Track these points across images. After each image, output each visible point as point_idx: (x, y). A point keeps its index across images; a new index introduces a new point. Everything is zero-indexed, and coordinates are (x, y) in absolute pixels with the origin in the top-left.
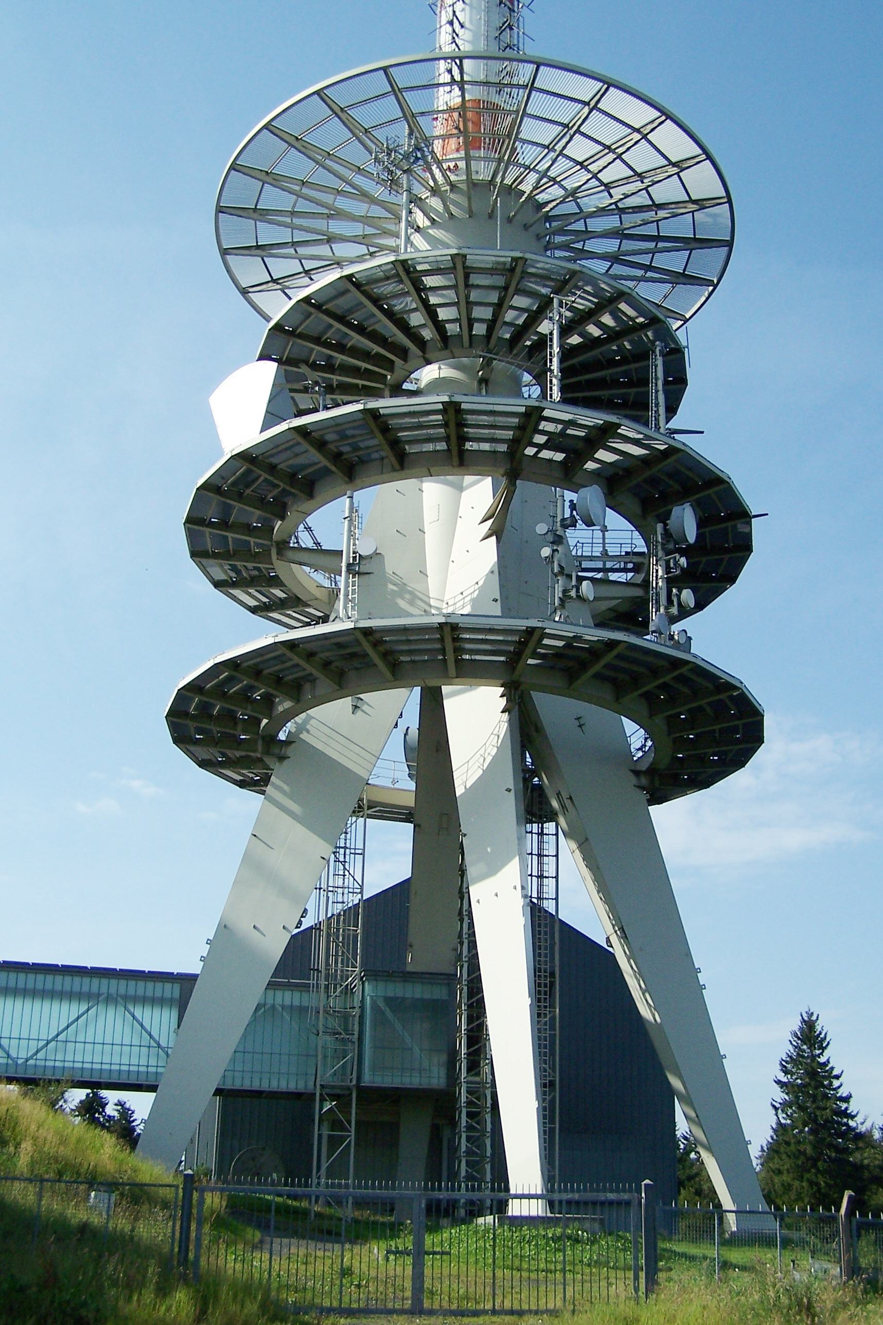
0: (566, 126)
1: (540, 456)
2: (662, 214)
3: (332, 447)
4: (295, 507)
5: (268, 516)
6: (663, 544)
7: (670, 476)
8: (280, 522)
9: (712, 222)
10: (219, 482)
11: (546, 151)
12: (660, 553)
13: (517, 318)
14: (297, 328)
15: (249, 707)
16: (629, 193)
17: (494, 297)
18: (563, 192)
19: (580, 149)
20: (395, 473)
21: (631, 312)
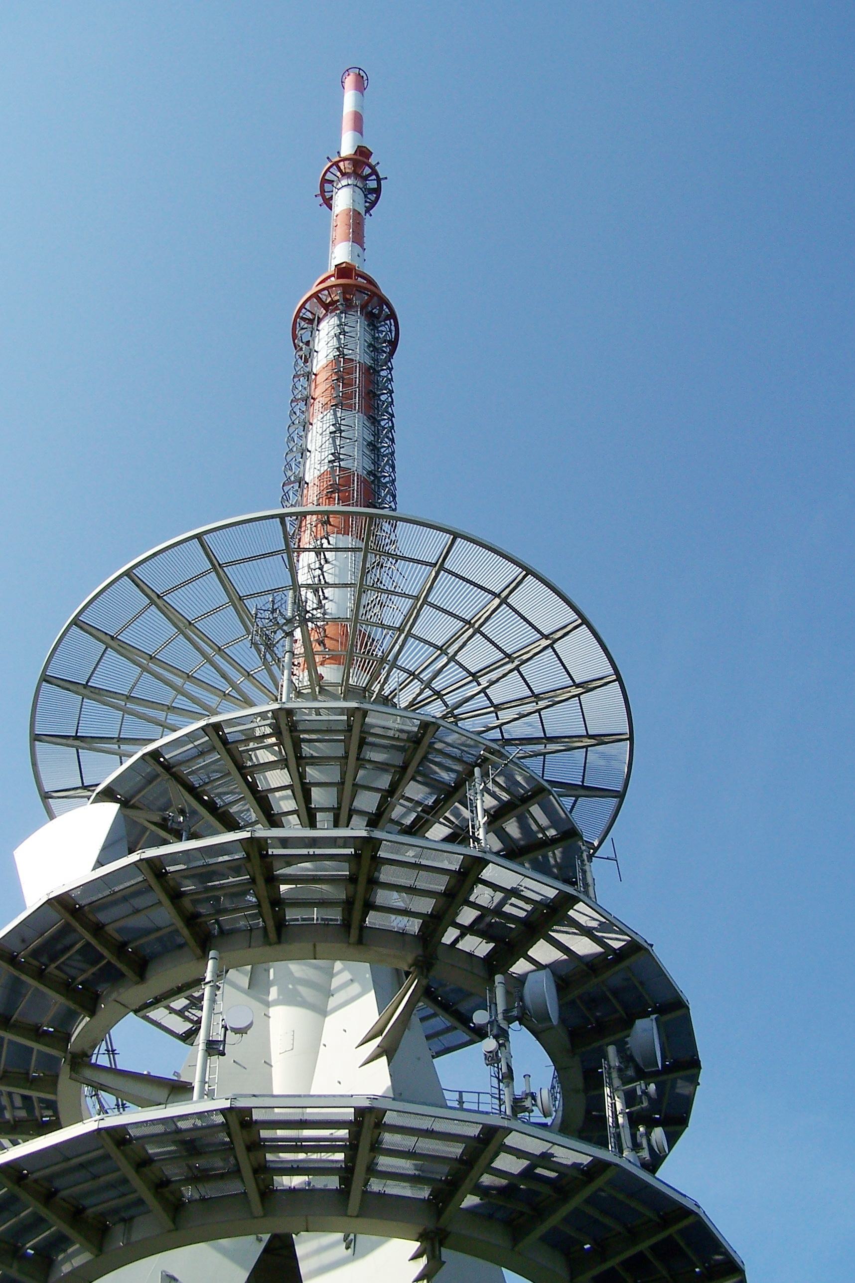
0: (468, 622)
1: (460, 946)
2: (552, 747)
3: (186, 902)
4: (114, 995)
5: (73, 1006)
6: (620, 1070)
7: (615, 992)
8: (88, 1019)
9: (606, 765)
10: (15, 946)
11: (439, 652)
12: (617, 1082)
13: (404, 815)
14: (133, 796)
15: (15, 1265)
16: (525, 713)
17: (384, 781)
18: (378, 796)
19: (477, 655)
20: (268, 948)
21: (544, 821)
